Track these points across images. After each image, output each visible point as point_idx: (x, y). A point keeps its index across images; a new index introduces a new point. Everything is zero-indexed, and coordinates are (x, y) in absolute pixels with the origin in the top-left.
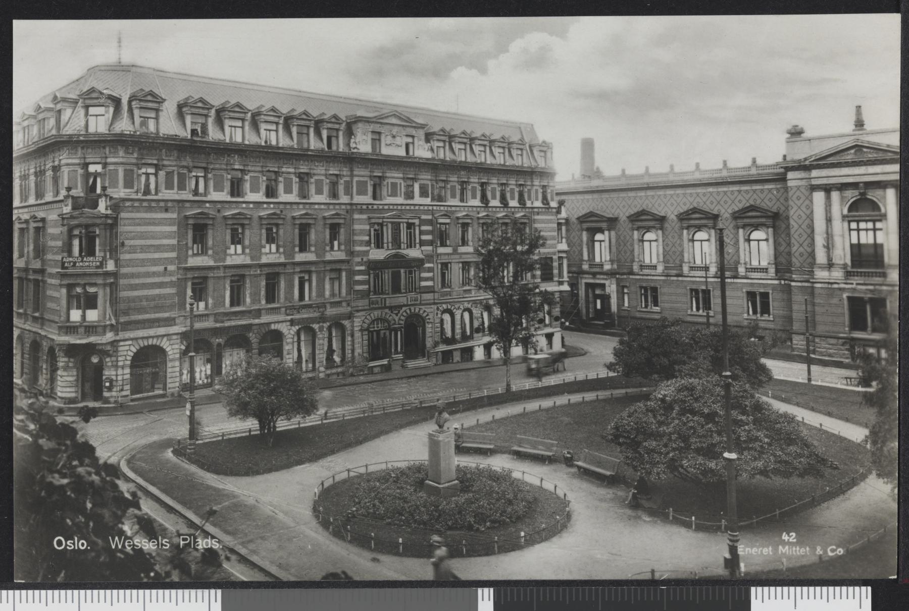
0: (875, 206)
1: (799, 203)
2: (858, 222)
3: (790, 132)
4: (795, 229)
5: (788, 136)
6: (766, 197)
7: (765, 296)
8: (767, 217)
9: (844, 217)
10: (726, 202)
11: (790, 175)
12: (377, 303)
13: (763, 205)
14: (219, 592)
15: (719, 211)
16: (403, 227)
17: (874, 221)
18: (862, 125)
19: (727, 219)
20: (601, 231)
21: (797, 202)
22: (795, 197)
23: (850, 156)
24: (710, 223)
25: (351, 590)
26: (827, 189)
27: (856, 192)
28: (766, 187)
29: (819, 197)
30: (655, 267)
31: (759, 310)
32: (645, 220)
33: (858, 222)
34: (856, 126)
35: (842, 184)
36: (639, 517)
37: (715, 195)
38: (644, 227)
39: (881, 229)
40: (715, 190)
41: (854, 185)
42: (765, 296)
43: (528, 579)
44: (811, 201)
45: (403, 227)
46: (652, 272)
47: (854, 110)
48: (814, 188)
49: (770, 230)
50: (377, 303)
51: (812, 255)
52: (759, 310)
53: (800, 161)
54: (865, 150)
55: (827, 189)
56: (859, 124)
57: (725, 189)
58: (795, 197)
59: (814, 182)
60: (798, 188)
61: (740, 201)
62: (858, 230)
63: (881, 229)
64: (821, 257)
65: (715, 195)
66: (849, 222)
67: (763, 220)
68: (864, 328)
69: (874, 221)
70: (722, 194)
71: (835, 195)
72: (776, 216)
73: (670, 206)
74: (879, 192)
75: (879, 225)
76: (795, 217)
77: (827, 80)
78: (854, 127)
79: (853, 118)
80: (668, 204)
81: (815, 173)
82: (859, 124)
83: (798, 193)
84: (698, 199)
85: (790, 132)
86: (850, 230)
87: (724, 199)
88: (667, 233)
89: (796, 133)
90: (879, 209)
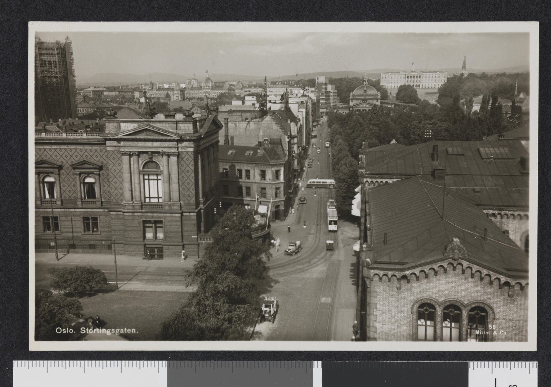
0: (157, 166)
2: (149, 175)
9: (140, 173)
10: (66, 156)
11: (108, 143)
13: (92, 161)
15: (102, 162)
17: (157, 175)
19: (68, 168)
21: (113, 161)
24: (96, 171)
26: (130, 155)
28: (53, 147)
29: (126, 158)
31: (202, 229)
33: (149, 175)
37: (68, 151)
40: (58, 147)
46: (94, 206)
48: (123, 154)
49: (97, 177)
52: (202, 229)
57: (66, 147)
59: (122, 150)
61: (76, 156)
62: (149, 179)
65: (99, 151)
66: (144, 175)
67: (93, 170)
68: (92, 221)
69: (157, 175)
70: (63, 151)
74: (160, 158)
75: (159, 177)
77: (501, 44)
80: (64, 156)
86: (144, 179)
90: (159, 168)
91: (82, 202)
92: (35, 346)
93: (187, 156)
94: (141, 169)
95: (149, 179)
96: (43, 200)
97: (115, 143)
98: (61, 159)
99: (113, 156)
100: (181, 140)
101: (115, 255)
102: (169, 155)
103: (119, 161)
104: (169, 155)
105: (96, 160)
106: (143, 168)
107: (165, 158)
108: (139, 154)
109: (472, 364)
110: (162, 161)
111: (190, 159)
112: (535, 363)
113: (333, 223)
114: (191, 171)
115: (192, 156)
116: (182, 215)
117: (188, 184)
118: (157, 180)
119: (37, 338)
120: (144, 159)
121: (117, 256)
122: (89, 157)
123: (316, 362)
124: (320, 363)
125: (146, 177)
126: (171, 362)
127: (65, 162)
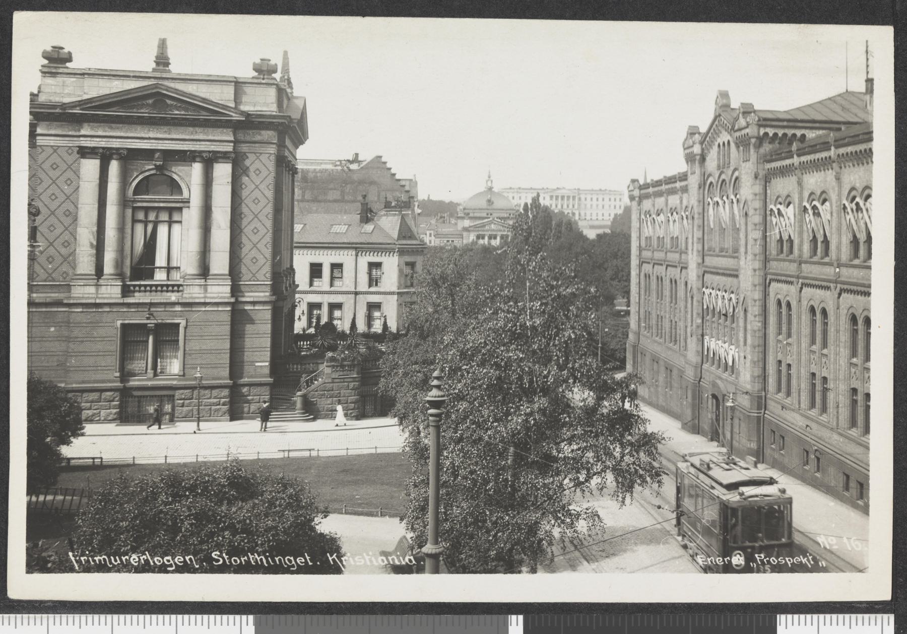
0: (175, 187)
1: (54, 174)
3: (46, 55)
4: (264, 242)
5: (46, 62)
14: (251, 617)
16: (667, 283)
18: (167, 64)
25: (308, 617)
26: (105, 156)
34: (158, 64)
36: (635, 347)
43: (893, 93)
44: (77, 173)
45: (667, 283)
47: (155, 44)
48: (84, 153)
53: (63, 106)
54: (169, 102)
55: (105, 156)
56: (162, 61)
66: (135, 209)
76: (263, 231)
78: (154, 65)
79: (154, 52)
83: (55, 158)
85: (46, 55)
86: (134, 221)
90: (179, 190)
92: (22, 583)
99: (55, 158)
101: (398, 293)
102: (209, 160)
103: (69, 174)
104: (209, 160)
106: (136, 192)
109: (782, 619)
111: (265, 173)
112: (892, 617)
113: (428, 563)
114: (263, 201)
119: (37, 563)
121: (396, 297)
123: (514, 617)
124: (521, 617)
125: (141, 216)
126: (263, 617)
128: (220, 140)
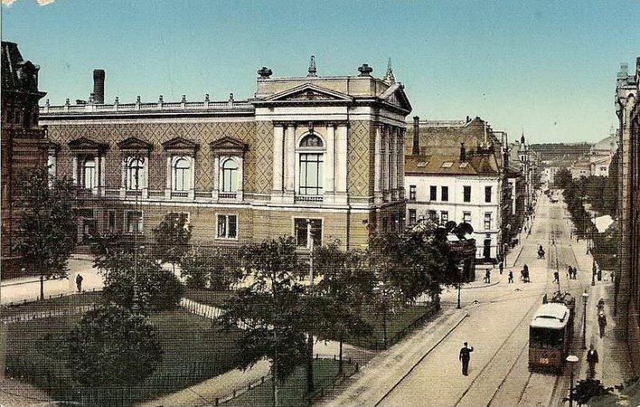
0: (320, 142)
3: (360, 69)
6: (234, 127)
7: (233, 219)
8: (239, 148)
11: (258, 111)
12: (488, 215)
20: (91, 158)
22: (261, 131)
23: (303, 99)
27: (307, 129)
30: (186, 195)
32: (135, 147)
35: (297, 122)
37: (197, 125)
38: (224, 154)
39: (142, 168)
41: (305, 123)
42: (317, 223)
46: (184, 199)
50: (488, 215)
51: (270, 182)
55: (285, 125)
56: (313, 71)
58: (261, 131)
60: (264, 122)
63: (142, 168)
64: (277, 185)
65: (197, 125)
66: (301, 154)
71: (290, 129)
72: (246, 148)
73: (157, 133)
75: (321, 158)
81: (277, 111)
82: (313, 71)
84: (230, 130)
85: (360, 69)
86: (301, 161)
87: (193, 130)
88: (247, 161)
89: (265, 73)
91: (295, 197)
93: (361, 127)
94: (298, 146)
95: (307, 161)
96: (297, 195)
97: (266, 110)
98: (249, 137)
100: (354, 104)
103: (270, 136)
104: (335, 124)
105: (242, 136)
107: (331, 130)
108: (296, 124)
110: (326, 134)
115: (368, 127)
116: (349, 214)
117: (360, 167)
118: (318, 162)
120: (303, 131)
122: (185, 134)
127: (203, 141)
128: (339, 113)
